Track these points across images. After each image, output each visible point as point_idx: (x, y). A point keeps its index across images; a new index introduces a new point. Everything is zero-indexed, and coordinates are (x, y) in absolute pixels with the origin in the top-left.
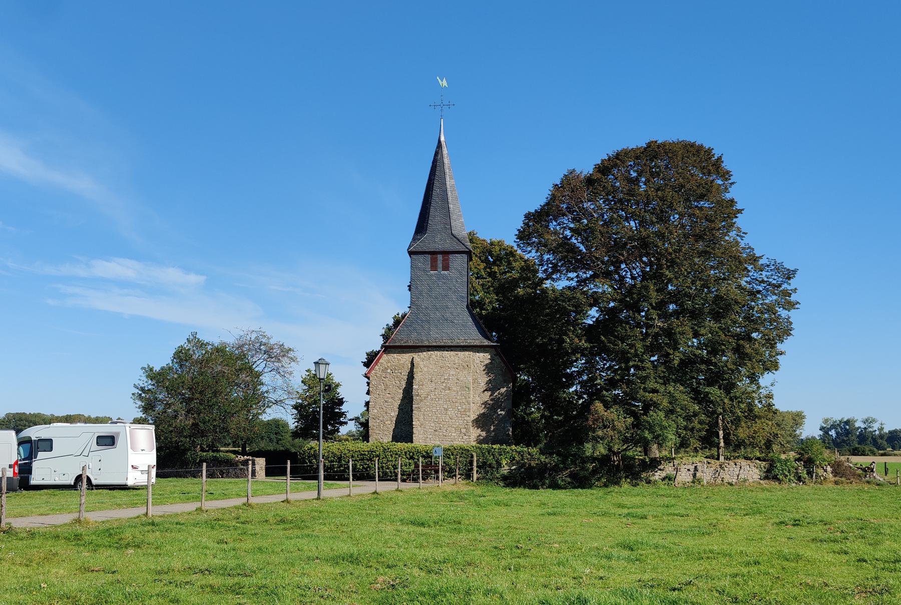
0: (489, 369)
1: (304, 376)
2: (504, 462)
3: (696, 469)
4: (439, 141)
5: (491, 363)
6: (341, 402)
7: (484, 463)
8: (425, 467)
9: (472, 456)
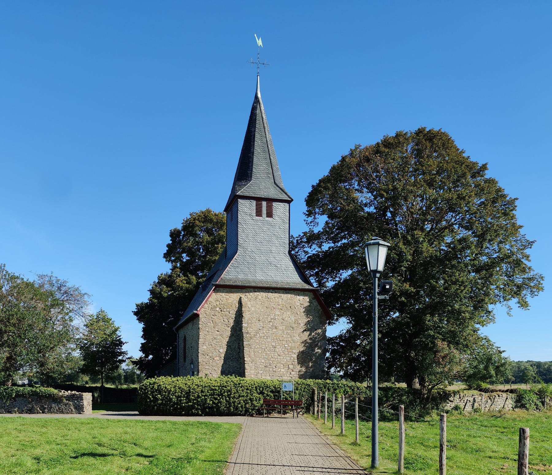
0: (308, 311)
3: (474, 400)
5: (309, 306)
6: (121, 343)
8: (274, 402)
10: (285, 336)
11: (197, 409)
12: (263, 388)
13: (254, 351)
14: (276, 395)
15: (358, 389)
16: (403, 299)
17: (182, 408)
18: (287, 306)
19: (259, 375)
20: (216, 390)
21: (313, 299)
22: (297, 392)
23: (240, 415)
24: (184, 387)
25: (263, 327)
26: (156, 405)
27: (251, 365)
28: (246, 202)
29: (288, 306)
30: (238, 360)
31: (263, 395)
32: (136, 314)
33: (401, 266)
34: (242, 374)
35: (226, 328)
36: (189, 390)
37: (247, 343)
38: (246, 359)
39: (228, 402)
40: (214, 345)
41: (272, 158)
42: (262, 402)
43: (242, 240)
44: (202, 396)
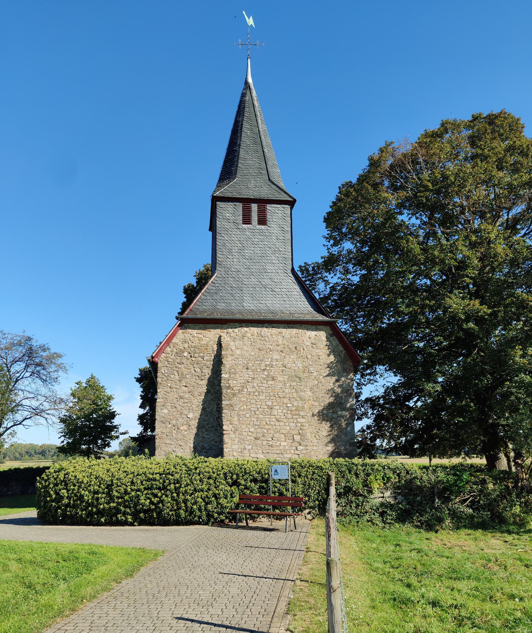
1: (73, 388)
2: (375, 486)
4: (246, 83)
6: (112, 415)
7: (348, 490)
8: (259, 499)
9: (329, 478)
10: (287, 391)
11: (125, 514)
12: (237, 475)
13: (239, 415)
14: (263, 487)
15: (408, 473)
16: (471, 325)
17: (100, 513)
18: (290, 346)
19: (246, 452)
20: (155, 480)
21: (331, 335)
22: (299, 480)
23: (199, 523)
24: (104, 477)
25: (254, 378)
26: (59, 508)
27: (233, 436)
28: (229, 206)
29: (292, 347)
30: (216, 430)
31: (238, 486)
32: (138, 380)
33: (463, 276)
34: (219, 453)
35: (198, 381)
36: (112, 481)
37: (228, 403)
38: (224, 427)
39: (176, 500)
40: (179, 408)
41: (266, 150)
42: (236, 499)
43: (222, 256)
44: (132, 490)
